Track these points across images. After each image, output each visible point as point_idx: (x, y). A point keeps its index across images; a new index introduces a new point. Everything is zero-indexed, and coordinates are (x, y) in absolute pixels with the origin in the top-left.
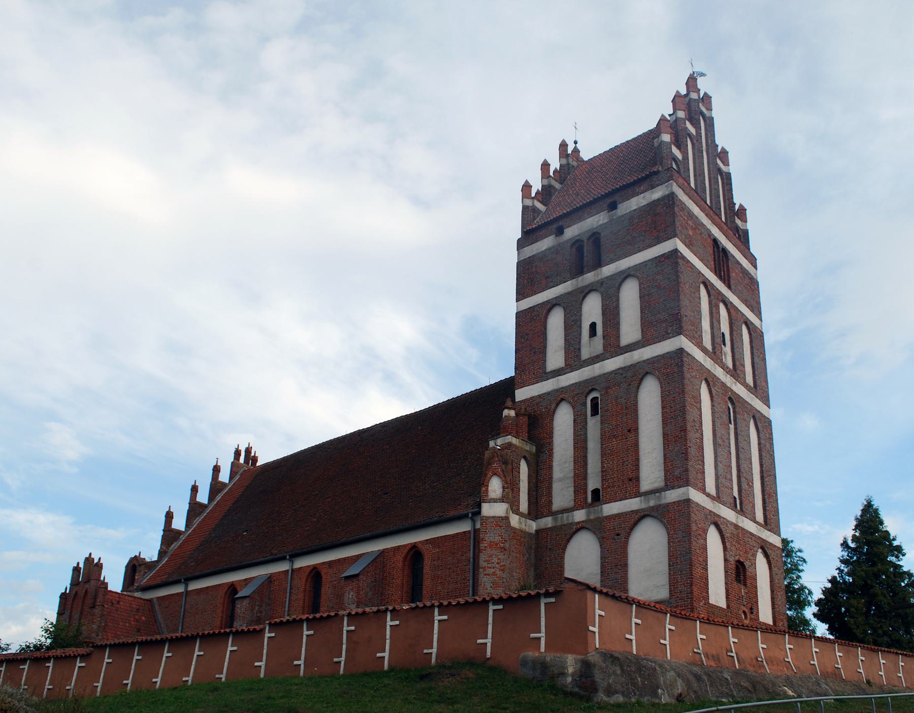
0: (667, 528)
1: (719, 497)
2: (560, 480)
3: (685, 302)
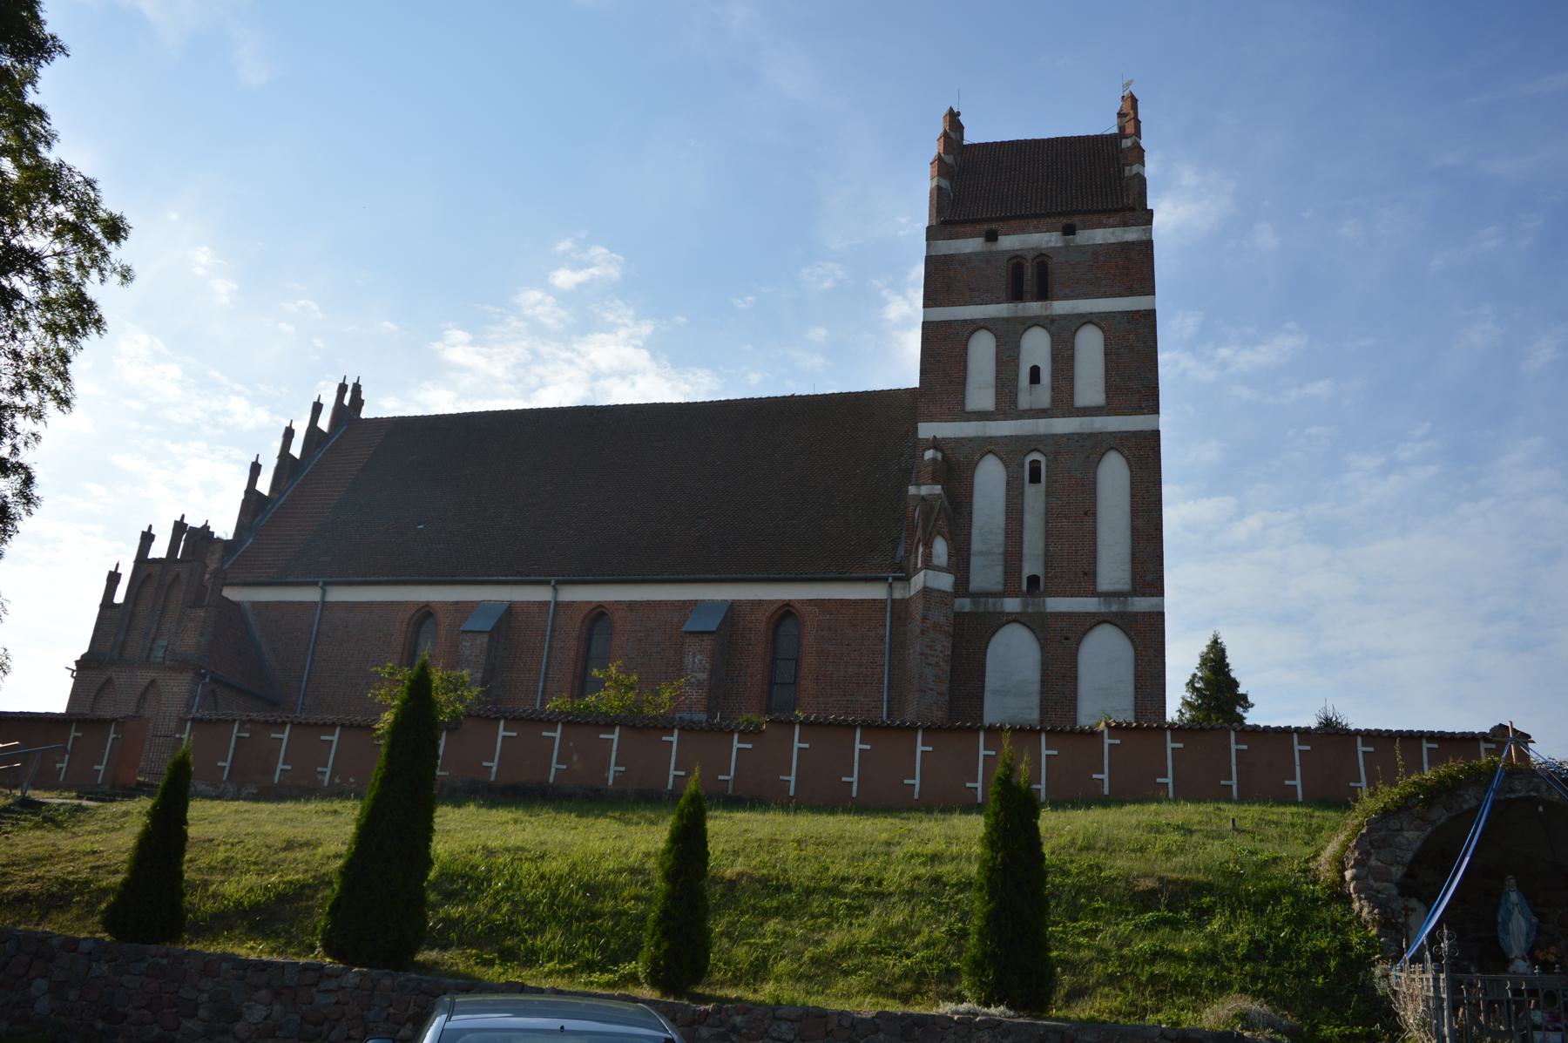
2: (981, 553)
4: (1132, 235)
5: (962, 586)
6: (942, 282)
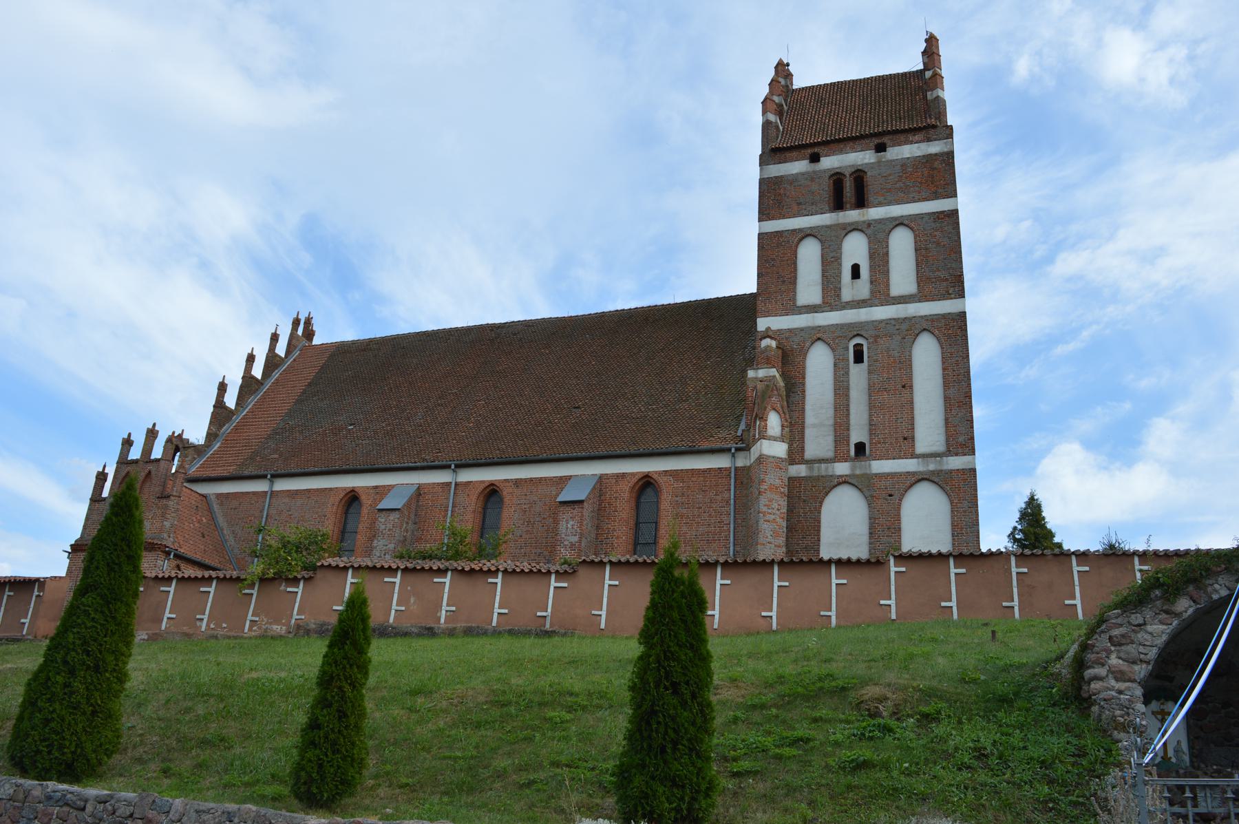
0: (949, 496)
2: (814, 426)
4: (935, 148)
5: (796, 454)
6: (773, 198)
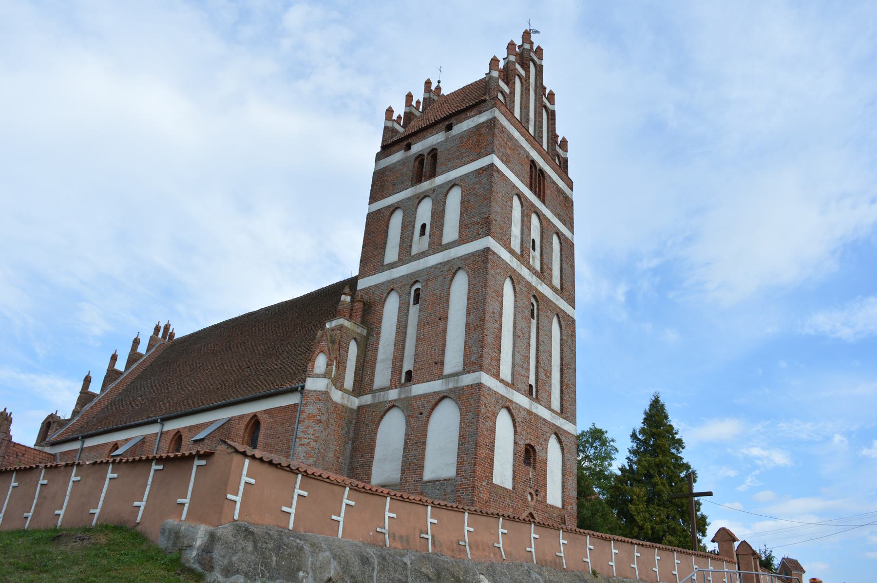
1: (513, 384)
2: (383, 361)
3: (496, 208)
